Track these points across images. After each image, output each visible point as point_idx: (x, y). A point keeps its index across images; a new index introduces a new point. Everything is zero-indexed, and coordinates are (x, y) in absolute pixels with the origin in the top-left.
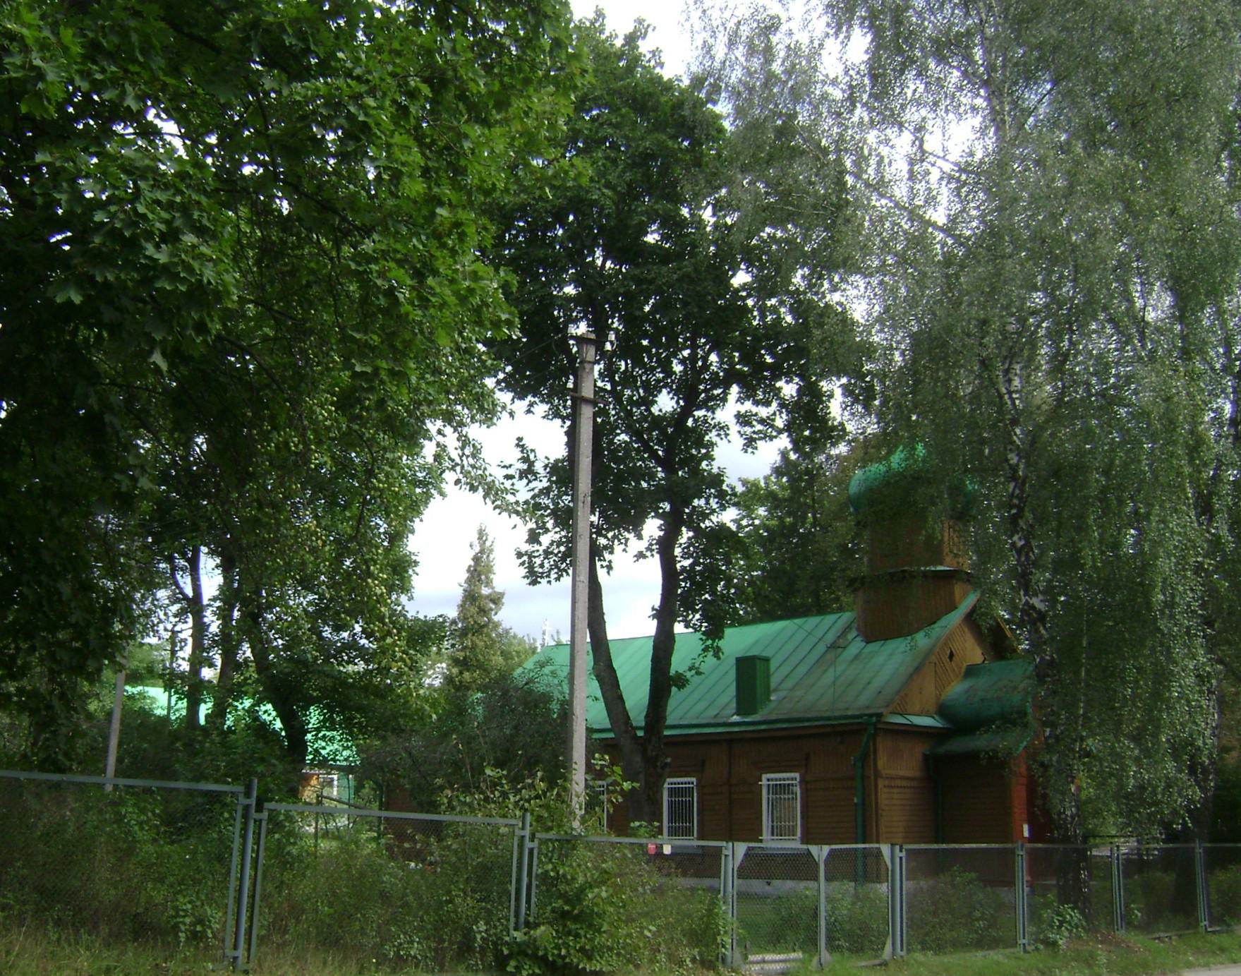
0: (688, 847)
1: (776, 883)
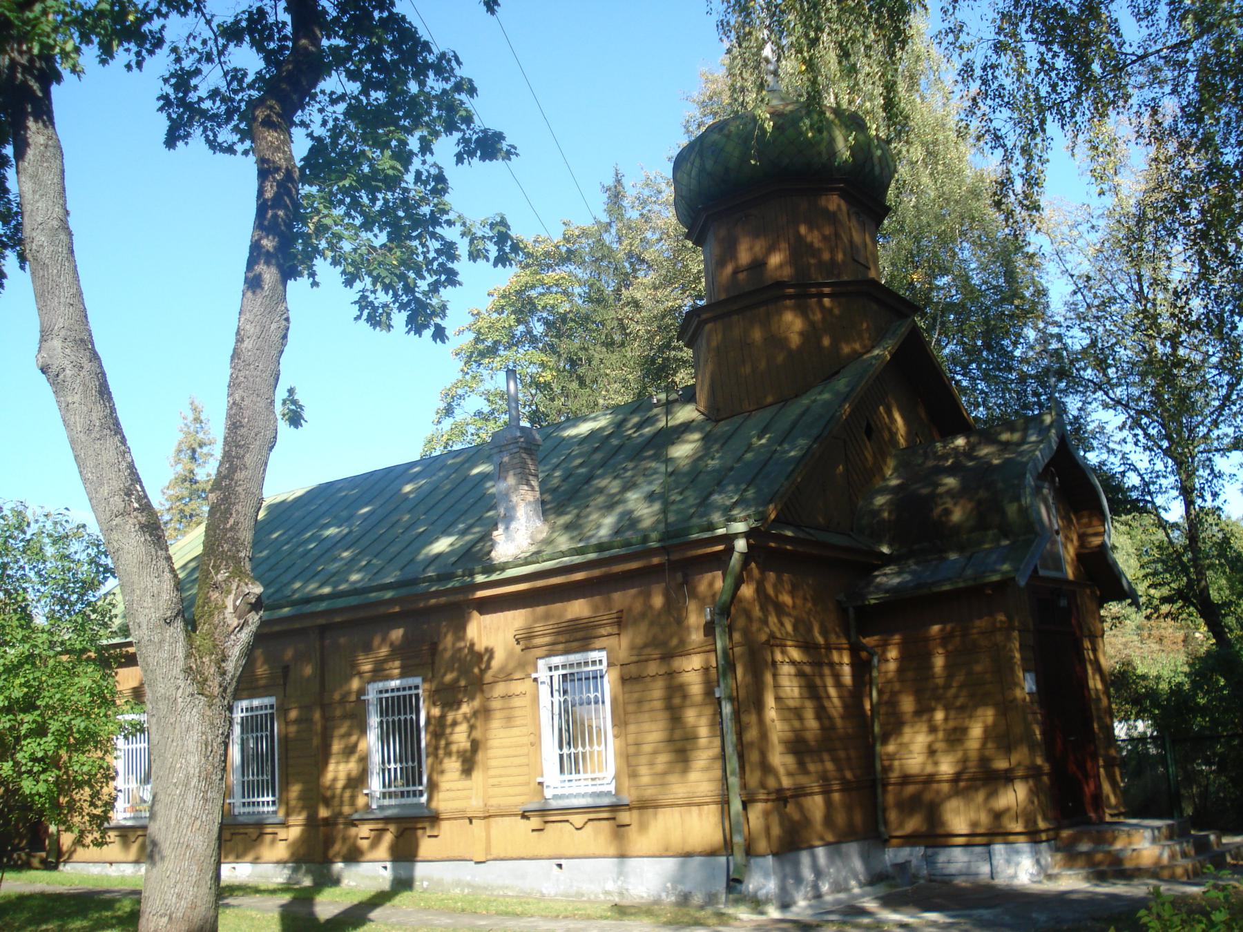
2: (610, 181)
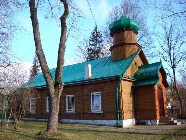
0: (71, 112)
1: (95, 121)
2: (95, 26)
